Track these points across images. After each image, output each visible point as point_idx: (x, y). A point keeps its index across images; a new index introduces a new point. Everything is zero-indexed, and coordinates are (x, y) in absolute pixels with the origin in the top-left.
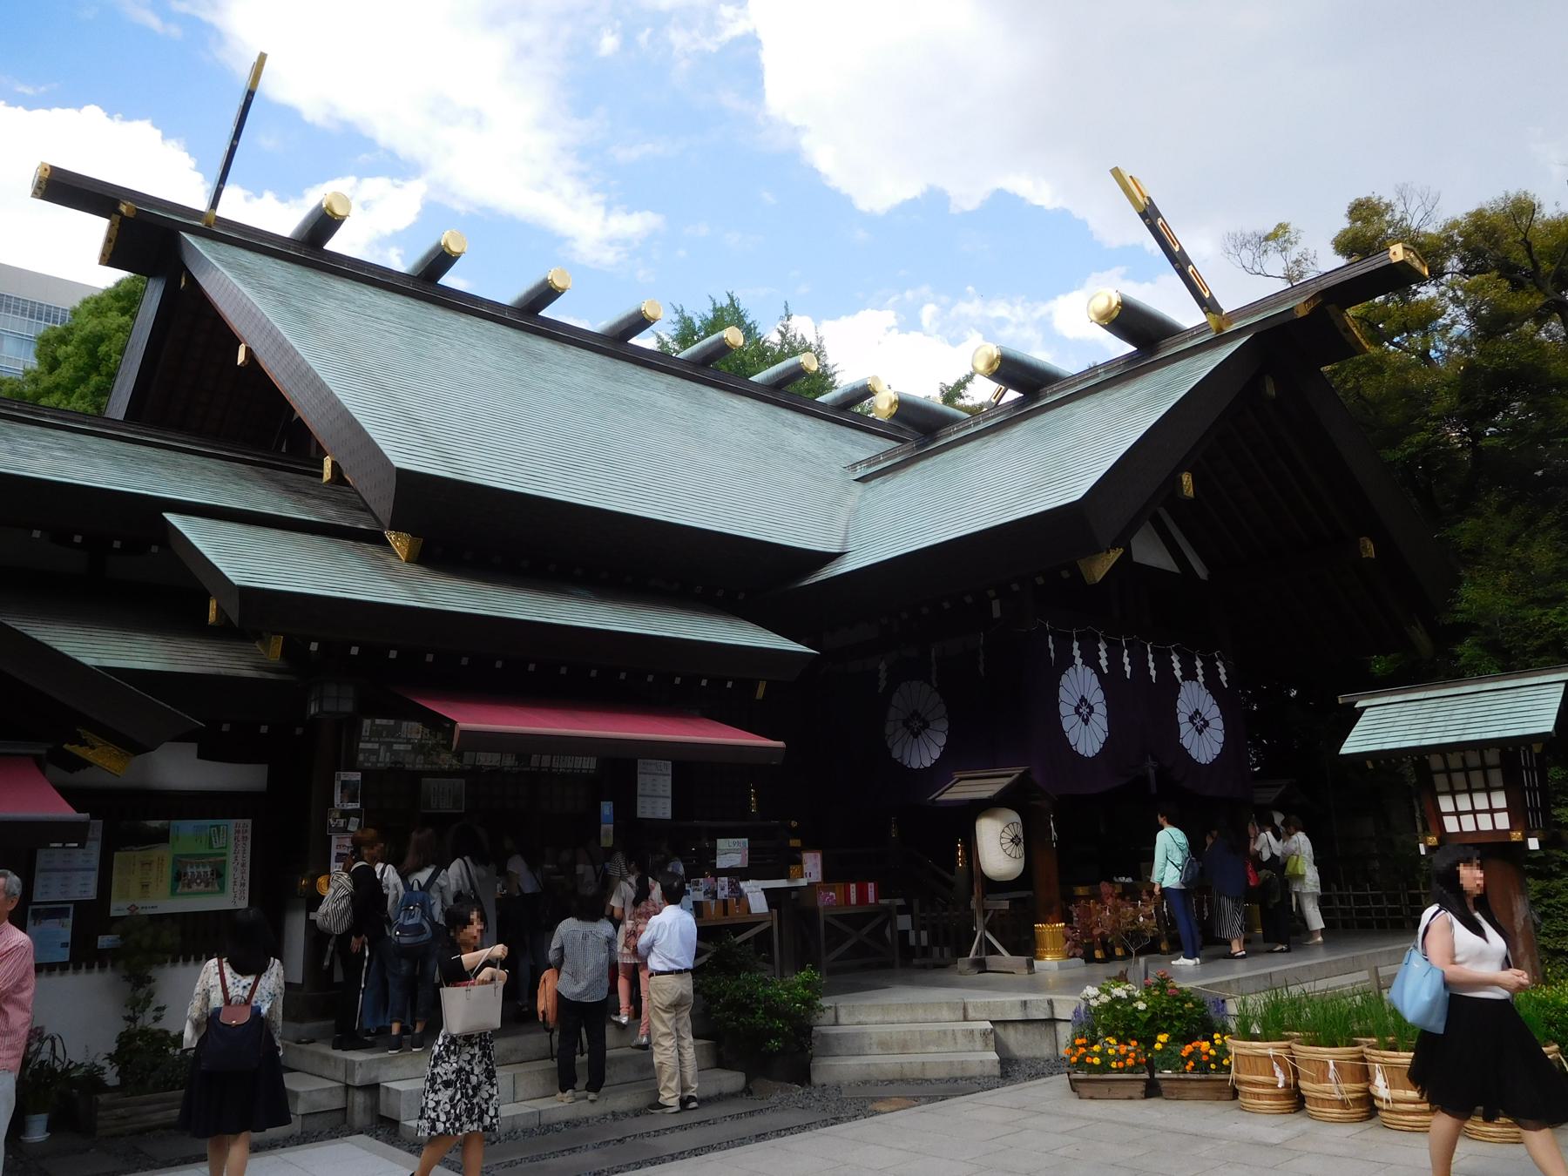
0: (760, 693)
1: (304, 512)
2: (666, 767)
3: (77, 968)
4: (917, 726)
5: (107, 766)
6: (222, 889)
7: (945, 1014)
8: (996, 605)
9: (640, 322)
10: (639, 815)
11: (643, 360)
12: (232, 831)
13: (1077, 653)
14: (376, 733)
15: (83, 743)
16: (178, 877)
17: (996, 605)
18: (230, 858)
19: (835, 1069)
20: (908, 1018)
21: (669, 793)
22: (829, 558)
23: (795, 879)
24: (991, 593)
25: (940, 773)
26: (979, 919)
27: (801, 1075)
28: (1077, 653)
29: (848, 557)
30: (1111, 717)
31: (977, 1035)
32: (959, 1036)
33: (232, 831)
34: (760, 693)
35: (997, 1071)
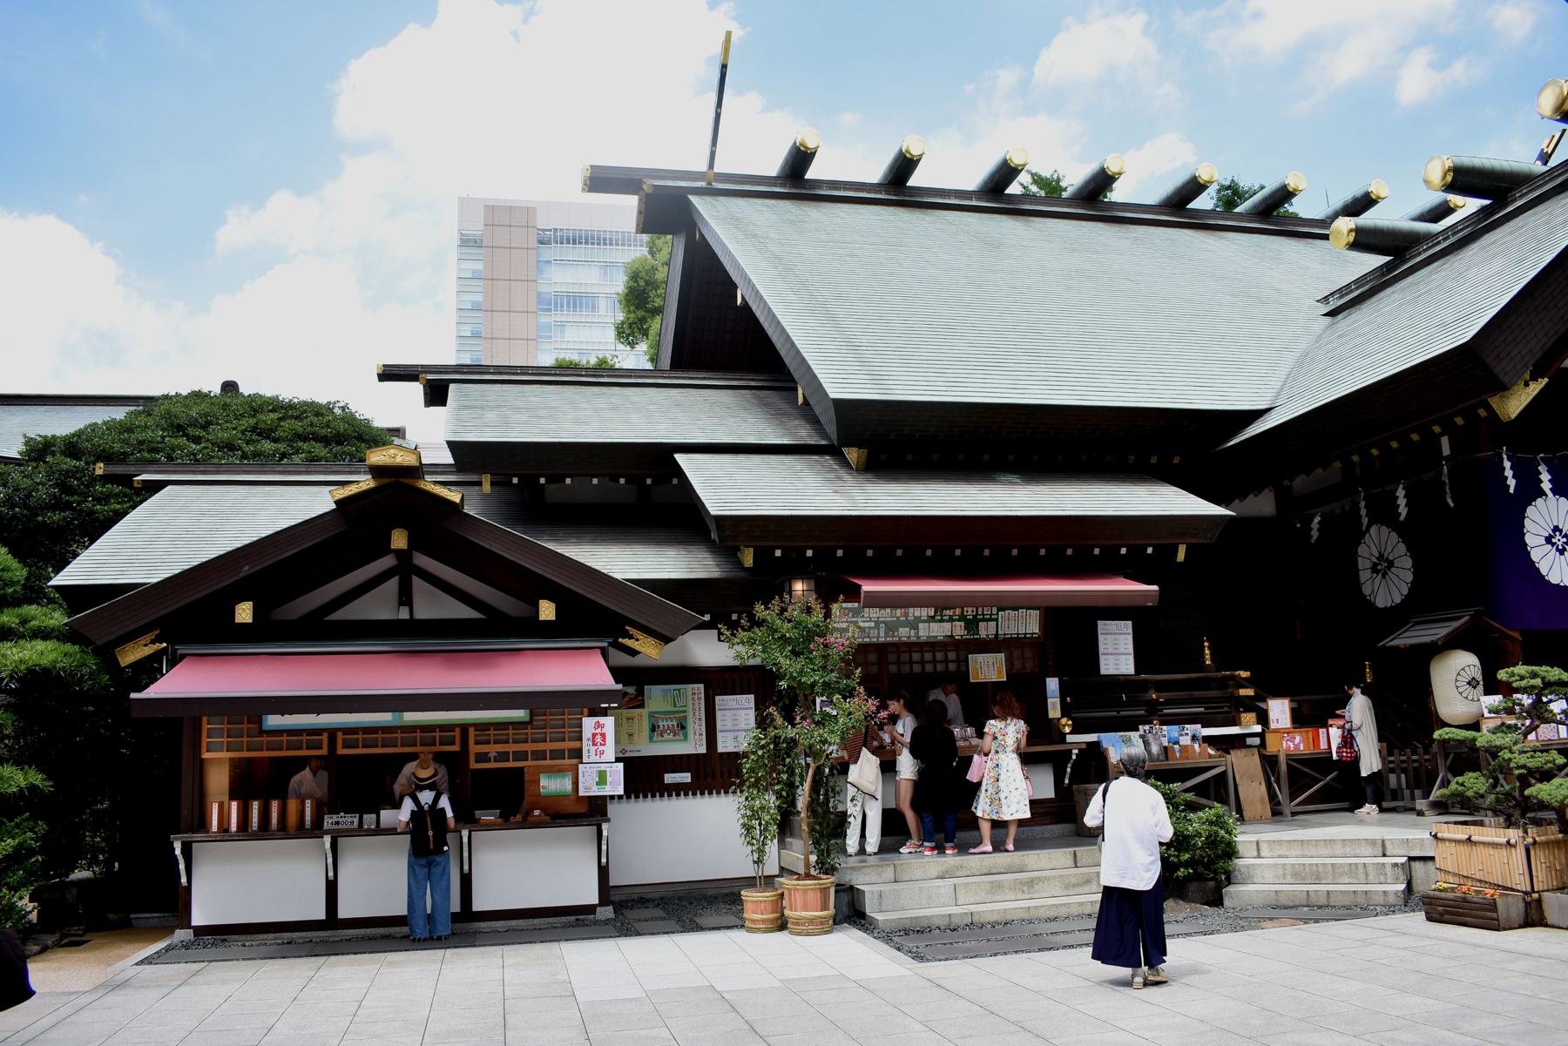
0: (1181, 557)
1: (783, 436)
2: (1127, 626)
3: (629, 797)
4: (1383, 566)
5: (649, 651)
6: (686, 737)
7: (1366, 850)
8: (1445, 441)
9: (1195, 187)
10: (1103, 672)
11: (1200, 223)
12: (690, 693)
13: (1545, 477)
14: (845, 612)
15: (631, 637)
16: (653, 729)
17: (1445, 441)
18: (690, 714)
19: (1233, 894)
20: (1327, 852)
21: (1131, 650)
22: (1256, 415)
23: (1248, 726)
24: (1437, 429)
25: (1399, 616)
26: (1440, 762)
27: (1216, 901)
28: (1545, 477)
29: (1273, 413)
30: (1354, 557)
31: (1389, 870)
32: (1370, 869)
33: (690, 693)
34: (1181, 557)
35: (1401, 902)
